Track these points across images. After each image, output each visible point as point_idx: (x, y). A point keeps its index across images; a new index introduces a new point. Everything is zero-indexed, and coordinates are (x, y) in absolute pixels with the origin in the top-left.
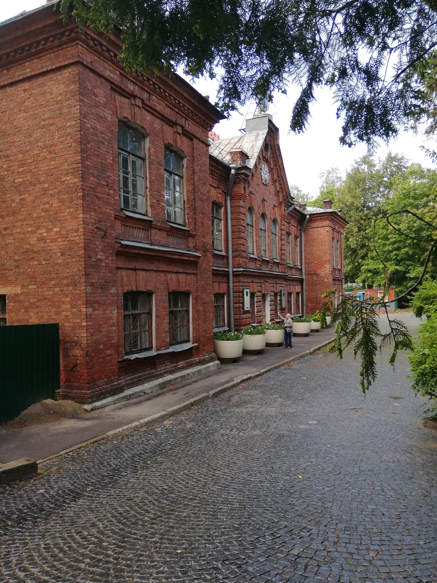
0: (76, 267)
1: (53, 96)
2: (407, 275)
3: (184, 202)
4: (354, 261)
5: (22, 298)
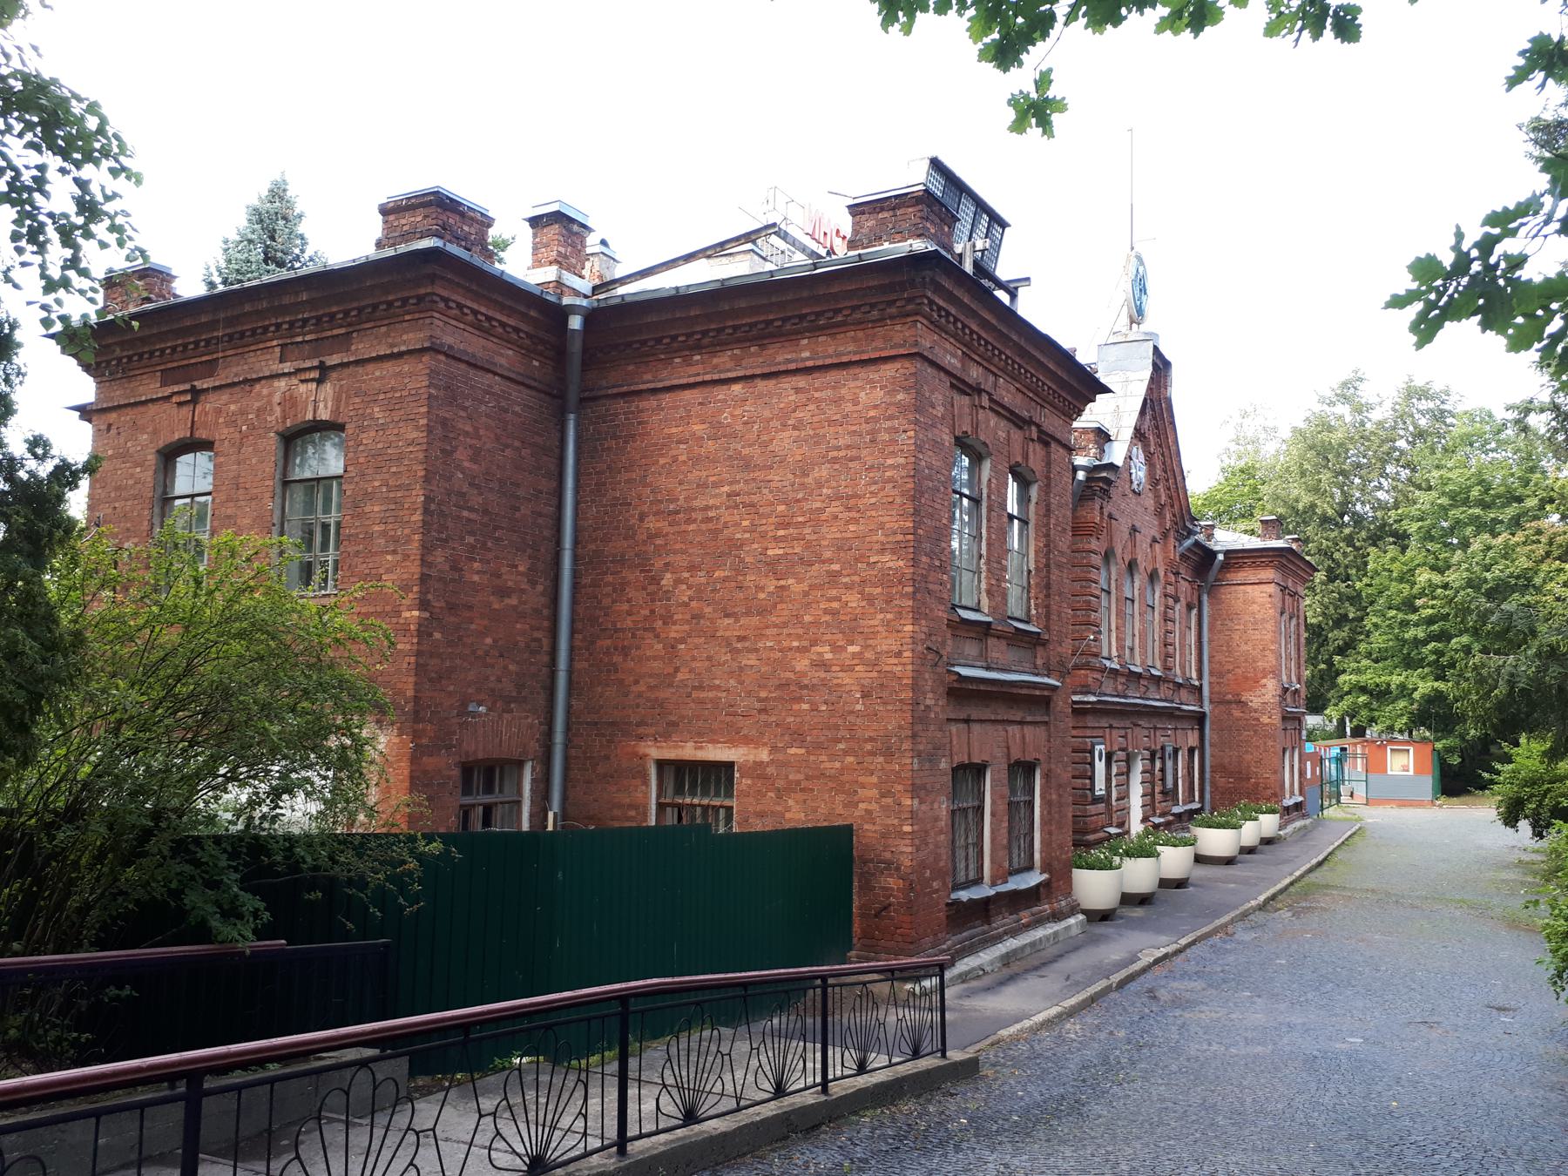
0: (894, 721)
1: (859, 408)
3: (1029, 572)
4: (1315, 658)
5: (770, 770)
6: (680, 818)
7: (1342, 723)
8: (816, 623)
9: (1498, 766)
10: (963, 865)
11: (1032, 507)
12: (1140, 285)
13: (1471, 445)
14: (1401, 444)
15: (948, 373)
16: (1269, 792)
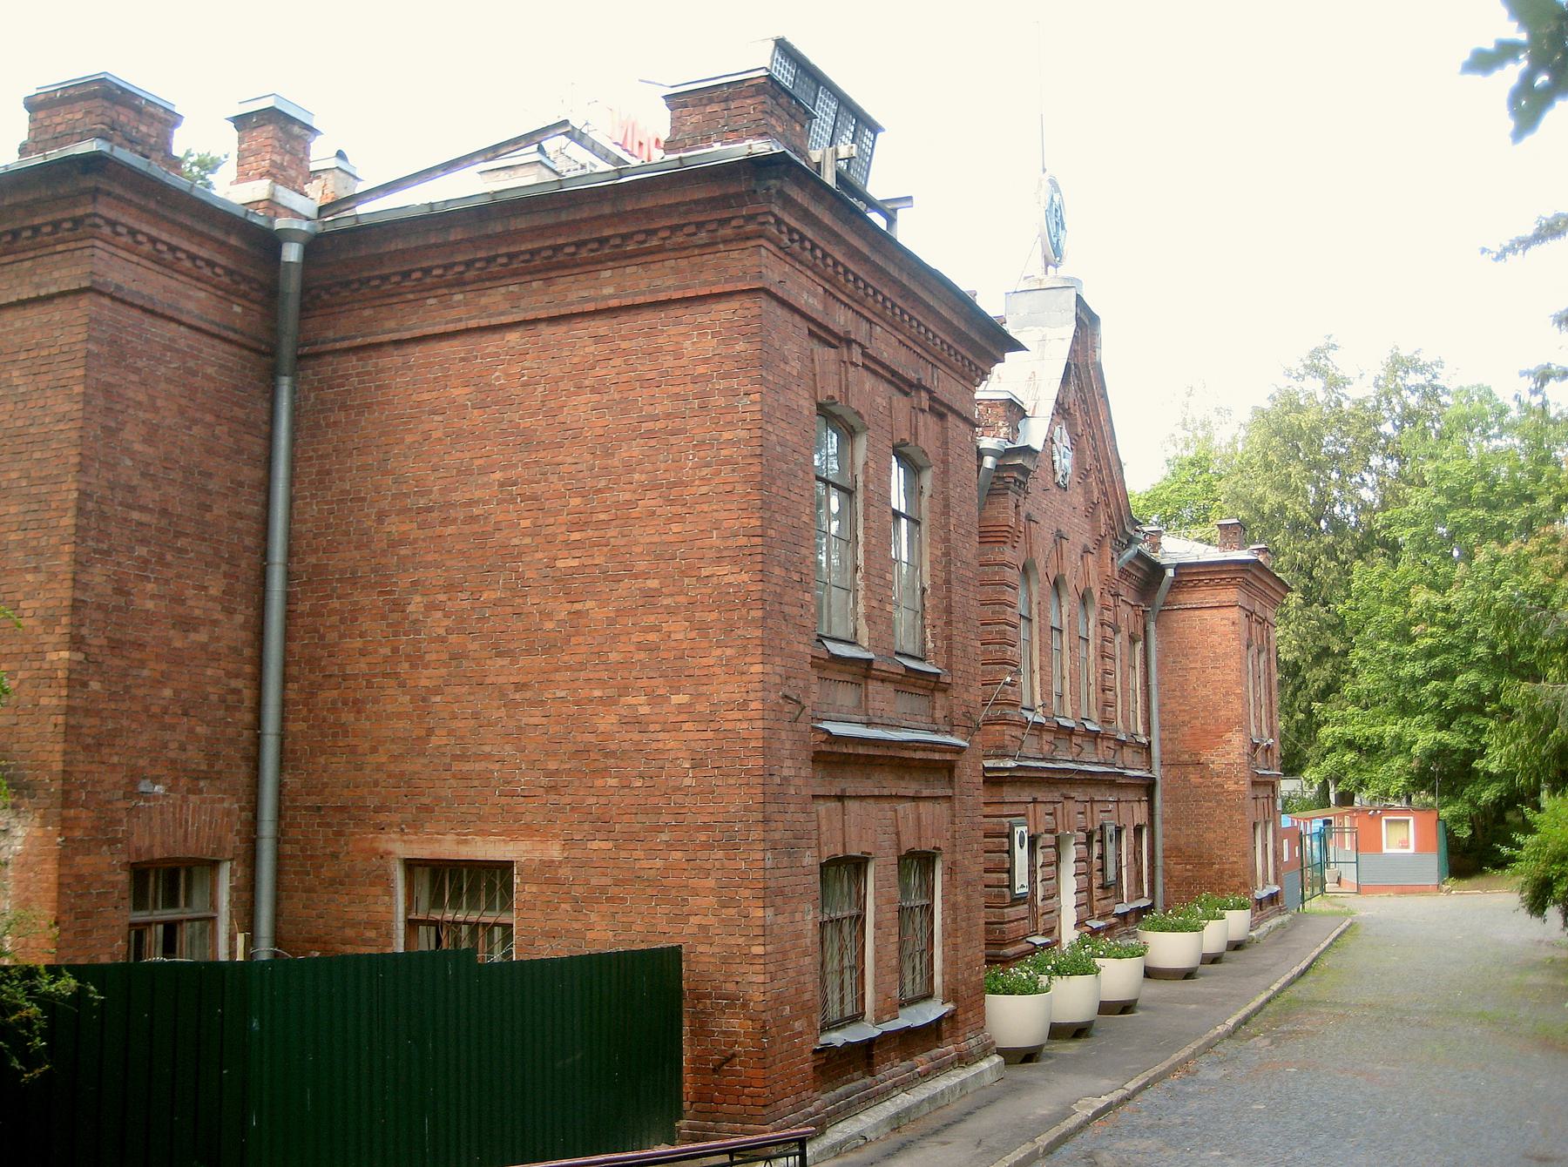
0: (737, 799)
2: (1478, 764)
3: (924, 590)
5: (564, 872)
6: (439, 941)
7: (1324, 787)
8: (626, 664)
9: (1520, 838)
10: (836, 996)
11: (925, 500)
12: (1056, 218)
13: (1471, 430)
14: (1387, 428)
15: (804, 316)
16: (1237, 881)
